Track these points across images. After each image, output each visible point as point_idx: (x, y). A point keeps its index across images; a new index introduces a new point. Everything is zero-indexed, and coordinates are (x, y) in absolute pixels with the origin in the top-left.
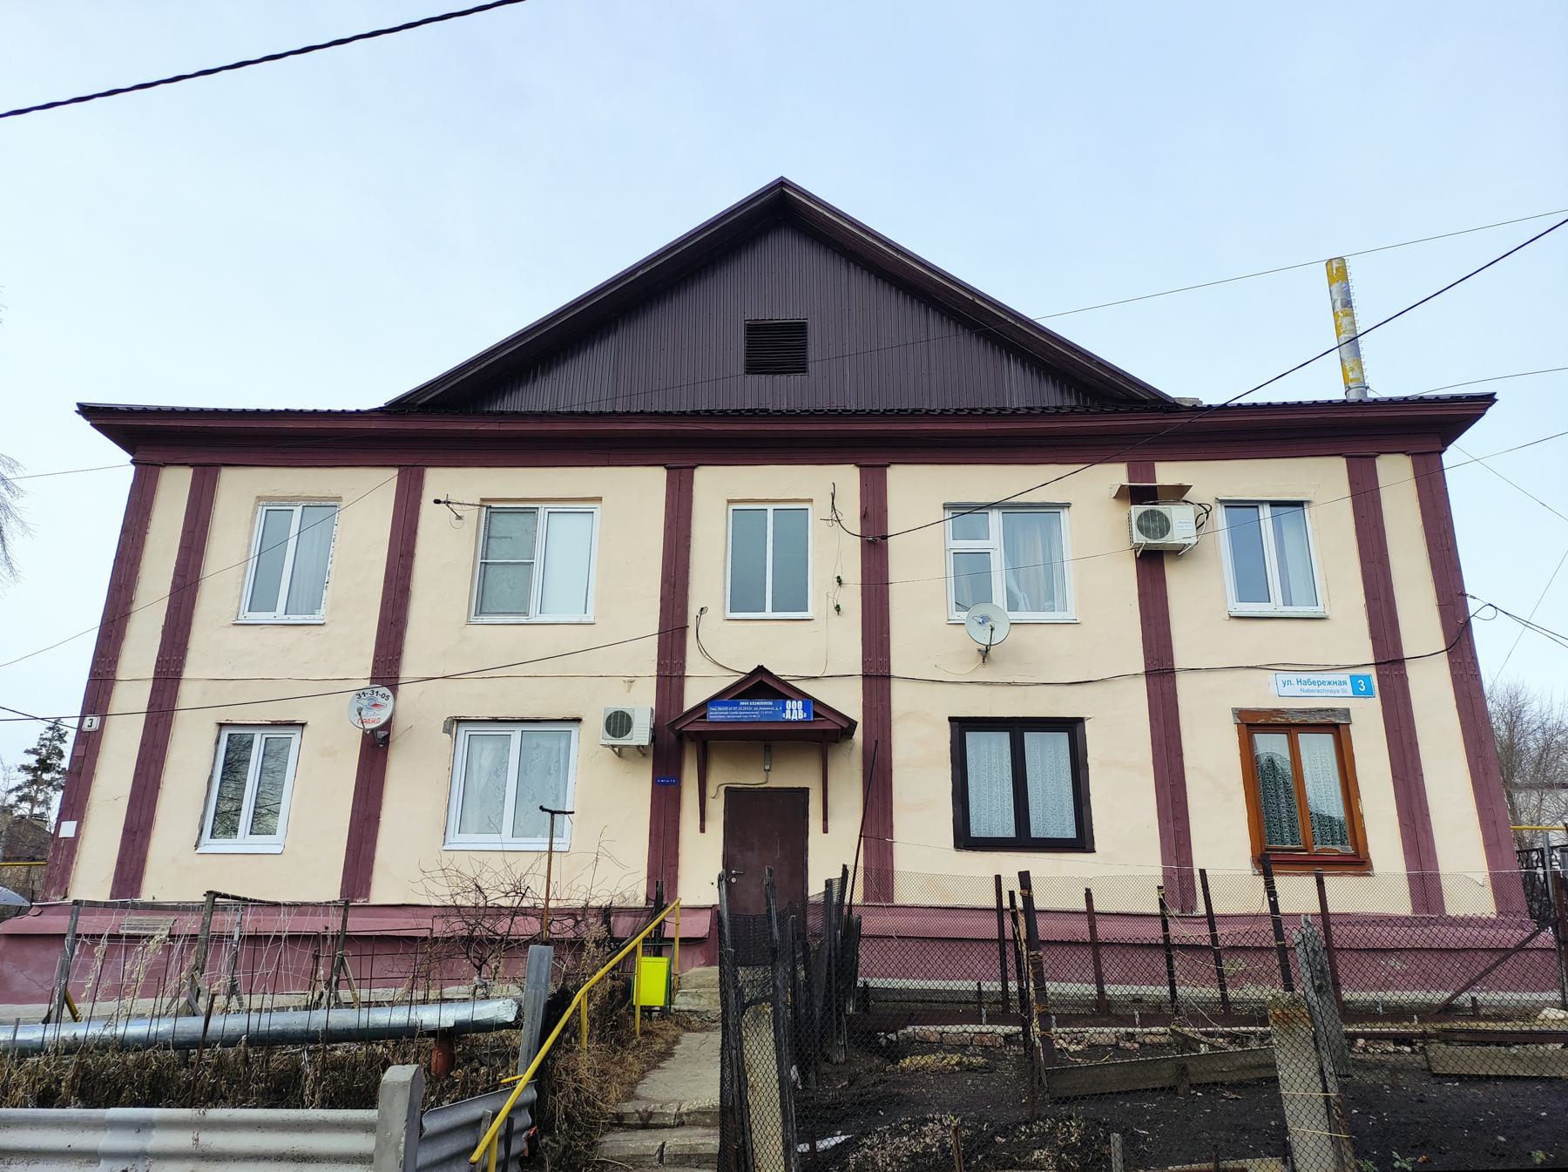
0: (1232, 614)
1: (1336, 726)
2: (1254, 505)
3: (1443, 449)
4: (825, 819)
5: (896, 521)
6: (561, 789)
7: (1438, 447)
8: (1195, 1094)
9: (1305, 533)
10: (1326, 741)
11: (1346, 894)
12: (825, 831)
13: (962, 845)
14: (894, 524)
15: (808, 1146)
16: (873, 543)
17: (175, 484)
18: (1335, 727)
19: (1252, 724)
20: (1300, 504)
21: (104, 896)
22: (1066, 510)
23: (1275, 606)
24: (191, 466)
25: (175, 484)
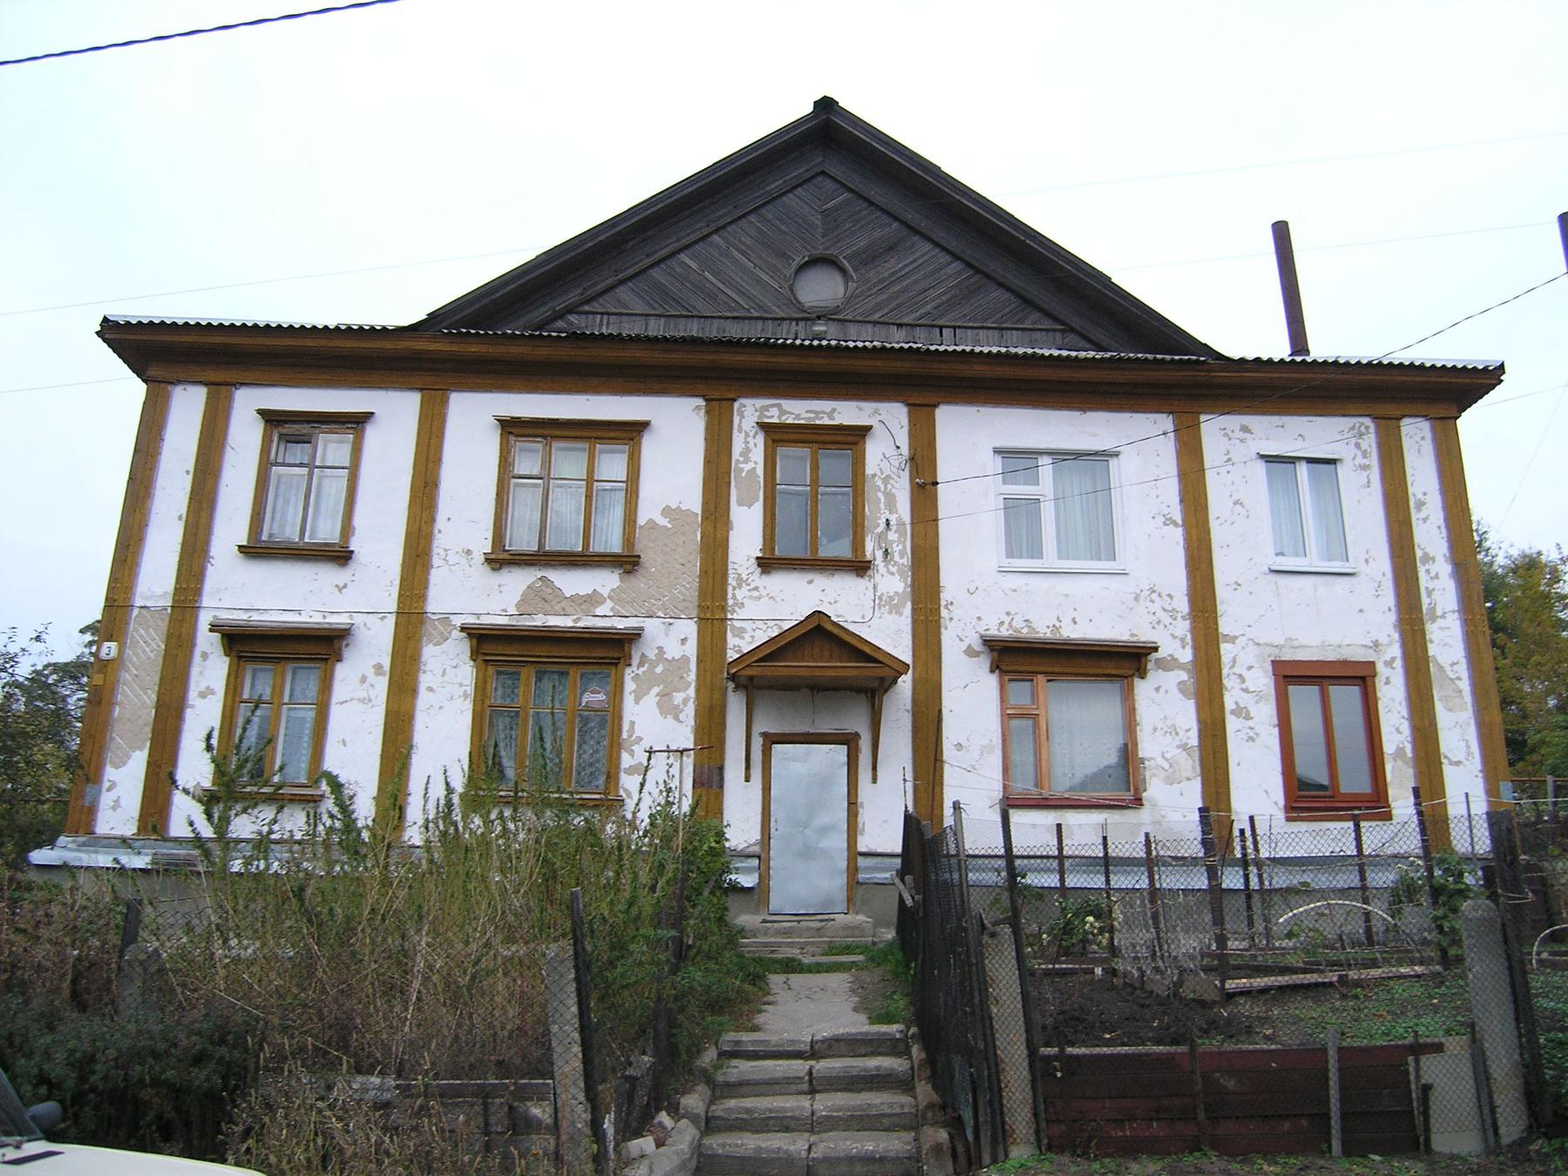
0: (1273, 568)
1: (1363, 678)
2: (1292, 460)
3: (1457, 415)
4: (874, 768)
5: (945, 468)
6: (890, 307)
7: (1454, 413)
8: (1055, 1069)
9: (1299, 519)
10: (1354, 692)
11: (1375, 836)
12: (874, 780)
13: (1181, 686)
14: (943, 472)
15: (1227, 986)
16: (922, 486)
17: (188, 404)
18: (1361, 677)
19: (1289, 675)
20: (1332, 462)
21: (130, 829)
22: (1115, 459)
23: (1313, 562)
24: (206, 384)
25: (188, 404)
